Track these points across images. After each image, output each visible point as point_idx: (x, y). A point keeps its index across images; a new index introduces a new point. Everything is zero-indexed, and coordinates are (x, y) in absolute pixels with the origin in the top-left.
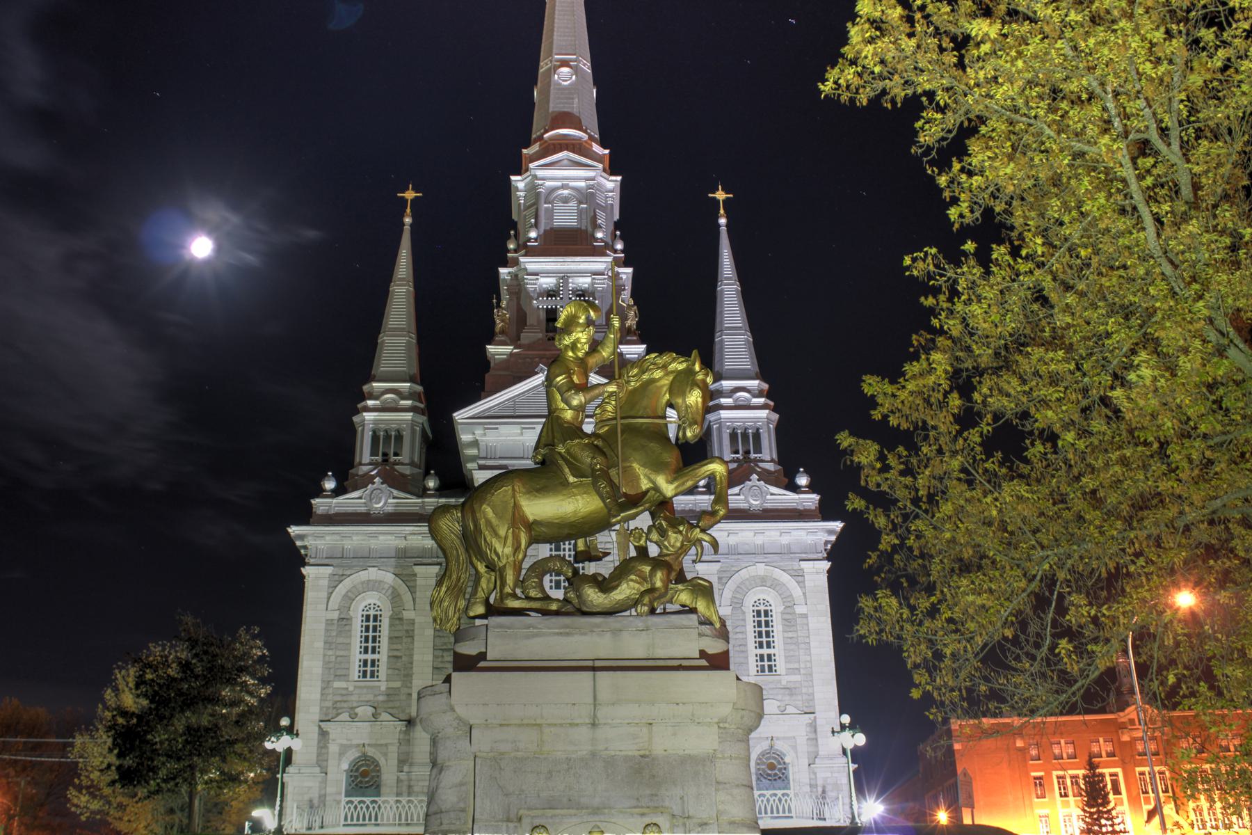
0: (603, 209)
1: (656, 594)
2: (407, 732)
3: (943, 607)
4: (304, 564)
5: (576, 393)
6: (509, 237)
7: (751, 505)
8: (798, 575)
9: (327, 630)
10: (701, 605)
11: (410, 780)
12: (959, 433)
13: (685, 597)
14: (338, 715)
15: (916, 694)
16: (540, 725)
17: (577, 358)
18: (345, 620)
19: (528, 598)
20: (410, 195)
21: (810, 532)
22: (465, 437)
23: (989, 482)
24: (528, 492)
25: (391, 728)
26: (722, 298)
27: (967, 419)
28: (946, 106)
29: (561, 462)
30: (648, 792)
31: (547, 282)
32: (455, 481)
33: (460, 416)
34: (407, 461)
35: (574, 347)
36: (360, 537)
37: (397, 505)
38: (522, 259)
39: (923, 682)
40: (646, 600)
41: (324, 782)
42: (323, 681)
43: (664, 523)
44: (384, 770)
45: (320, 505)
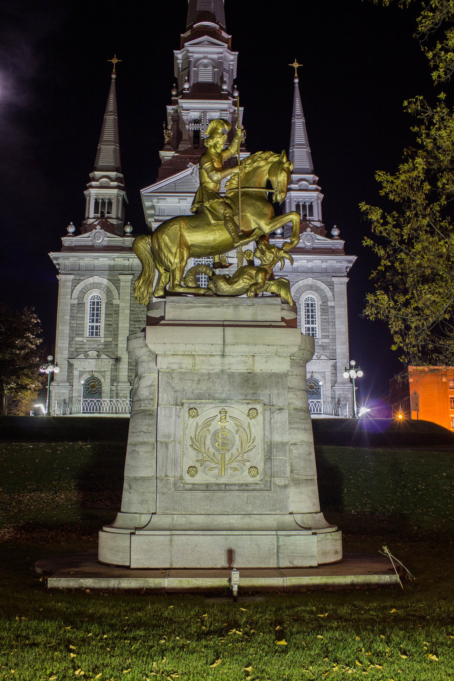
0: (228, 72)
1: (258, 286)
2: (115, 365)
3: (412, 301)
4: (58, 273)
5: (216, 173)
6: (173, 87)
7: (306, 245)
8: (331, 285)
9: (71, 310)
10: (283, 293)
11: (117, 390)
12: (428, 205)
13: (274, 288)
14: (78, 355)
15: (394, 348)
16: (194, 355)
17: (217, 153)
18: (81, 305)
19: (188, 287)
20: (115, 61)
21: (338, 261)
22: (147, 204)
23: (442, 233)
24: (188, 229)
25: (106, 364)
26: (294, 126)
27: (432, 197)
28: (436, 7)
29: (207, 212)
30: (251, 392)
31: (195, 115)
32: (142, 229)
33: (144, 191)
34: (115, 217)
35: (215, 146)
36: (89, 259)
37: (109, 241)
38: (180, 101)
39: (398, 342)
40: (253, 289)
41: (72, 390)
42: (70, 337)
43: (264, 247)
44: (103, 384)
45: (67, 241)
